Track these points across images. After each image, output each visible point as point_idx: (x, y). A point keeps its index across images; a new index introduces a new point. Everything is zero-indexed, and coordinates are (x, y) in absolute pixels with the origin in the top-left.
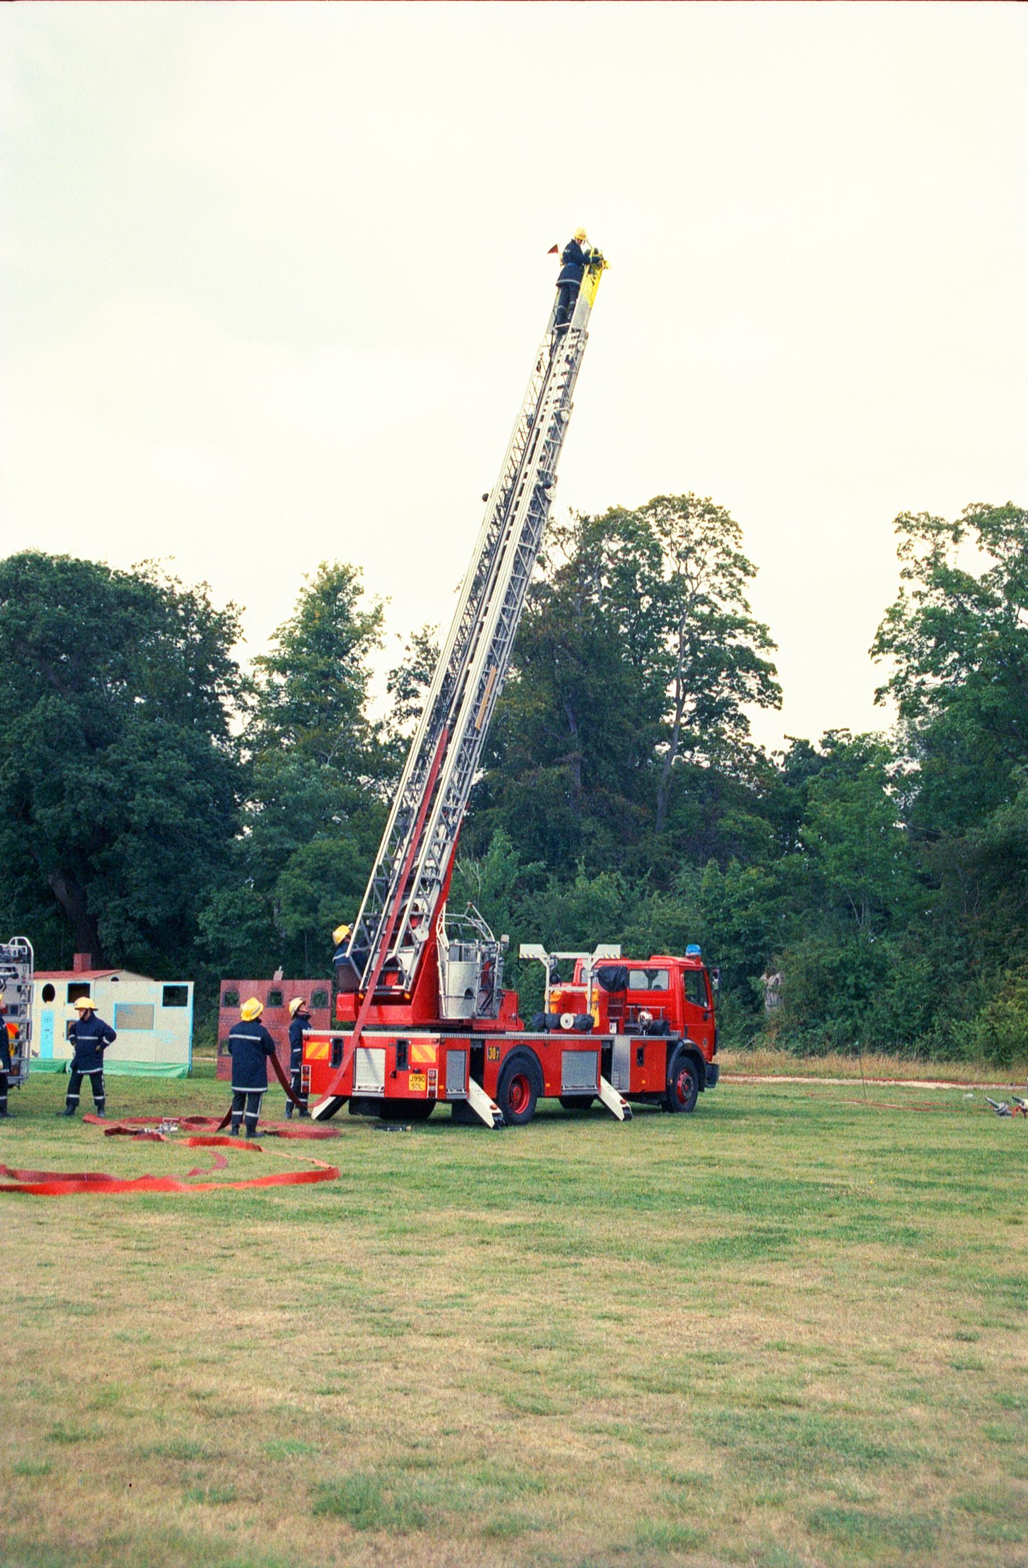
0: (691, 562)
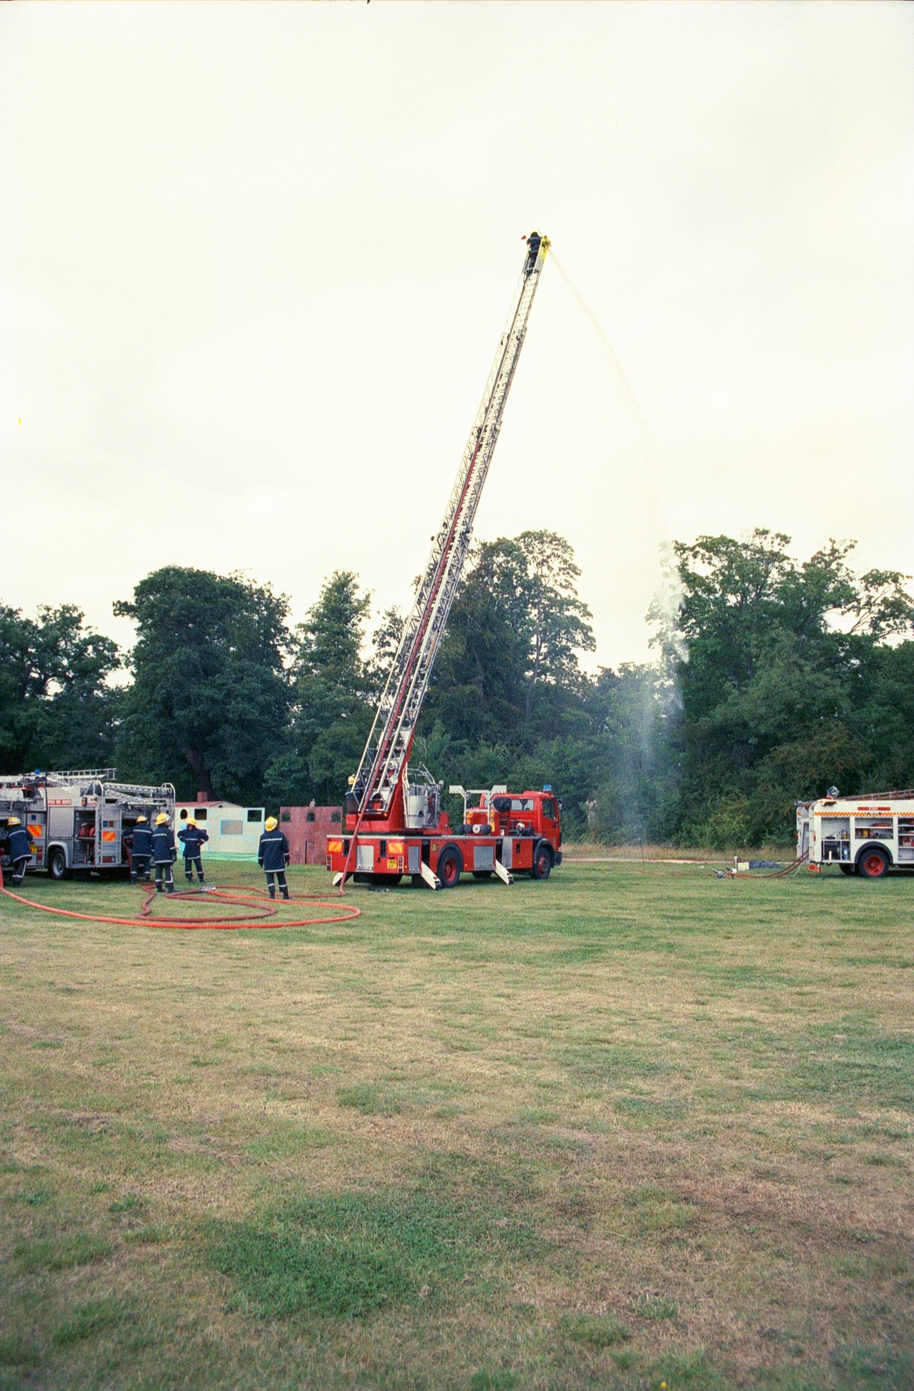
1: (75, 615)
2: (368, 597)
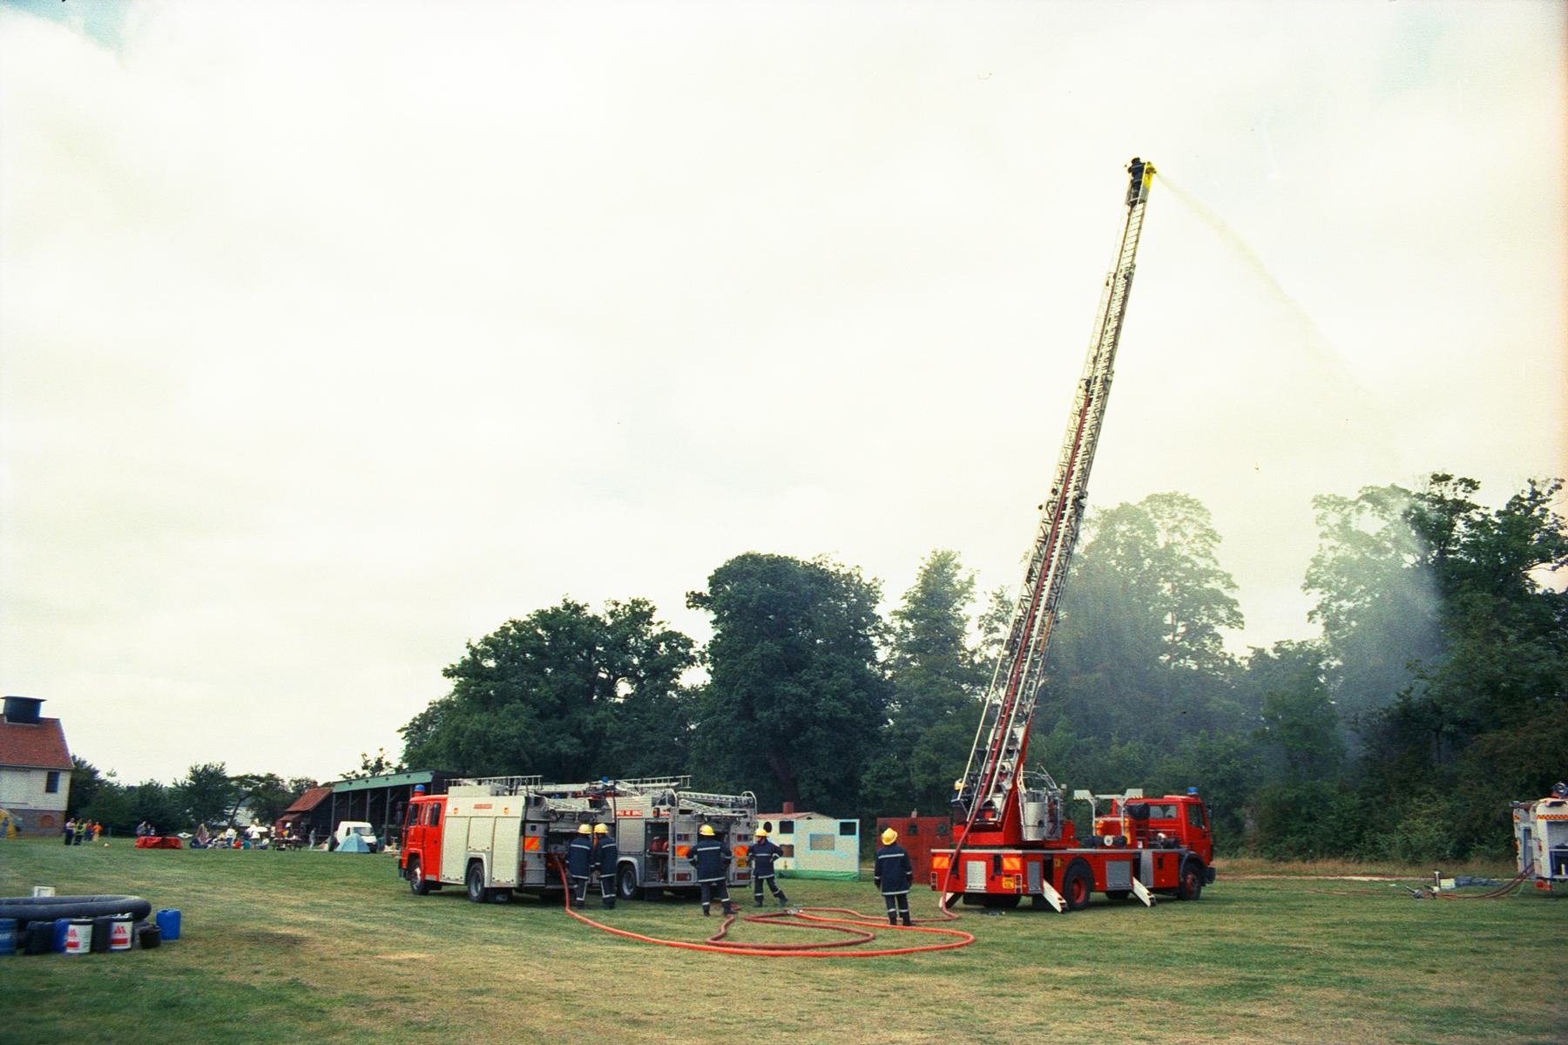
1: (646, 609)
2: (971, 578)
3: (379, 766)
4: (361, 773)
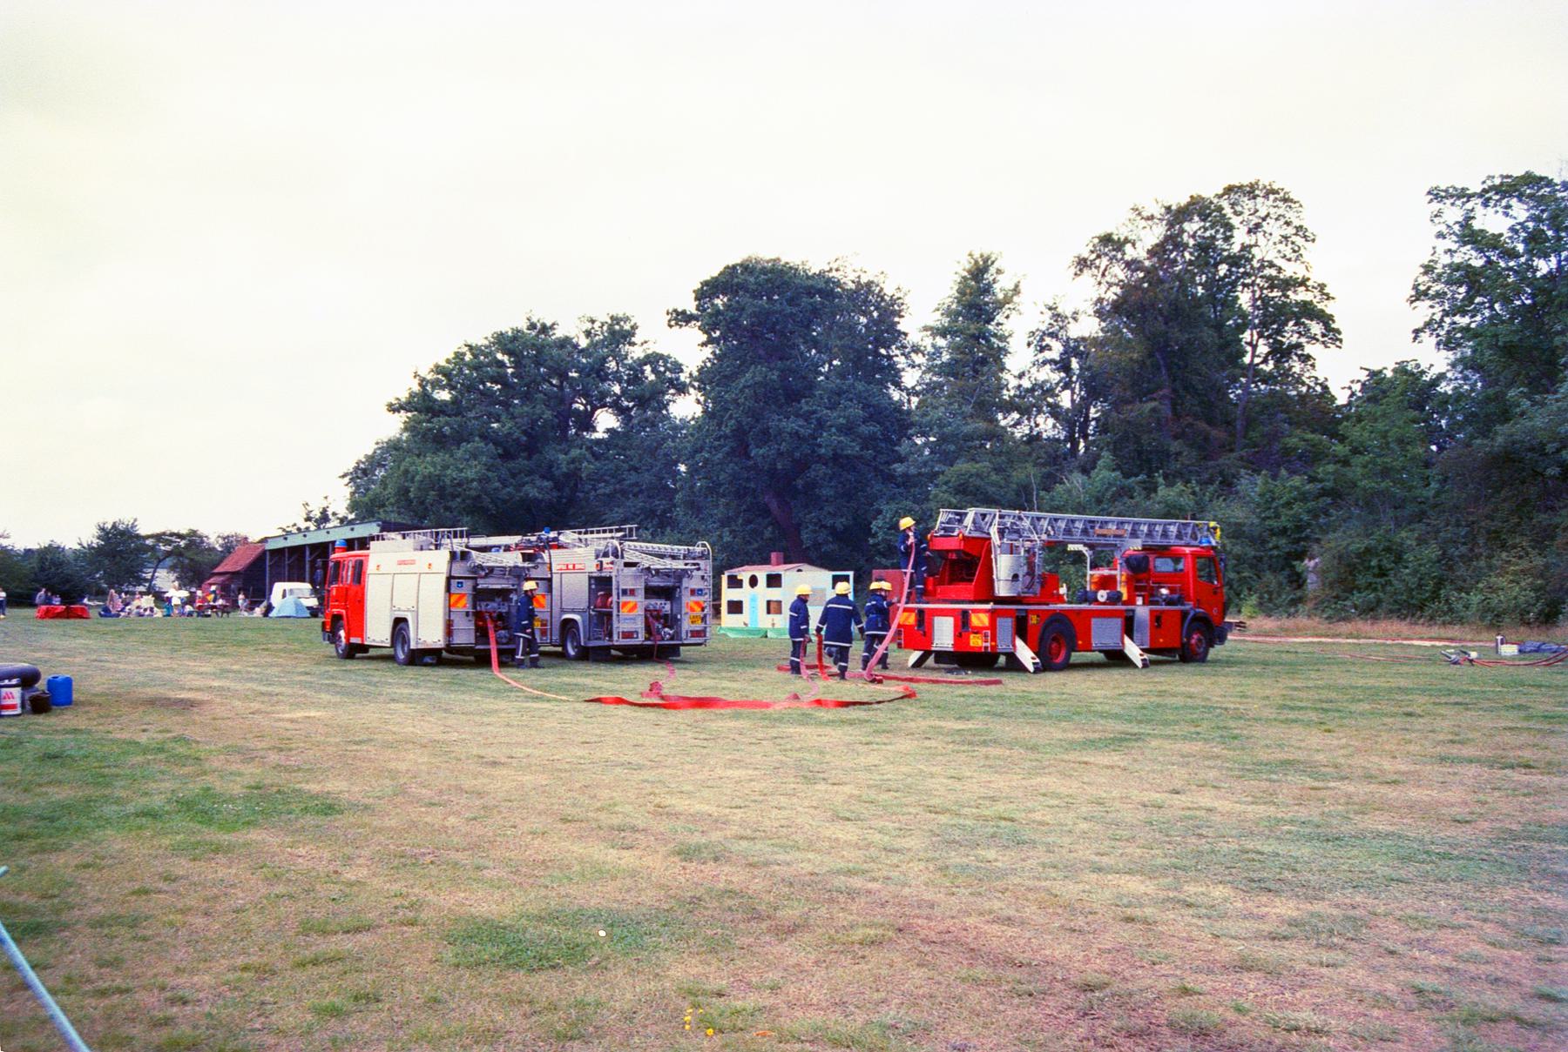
0: (1260, 235)
1: (627, 327)
3: (324, 518)
4: (303, 525)
